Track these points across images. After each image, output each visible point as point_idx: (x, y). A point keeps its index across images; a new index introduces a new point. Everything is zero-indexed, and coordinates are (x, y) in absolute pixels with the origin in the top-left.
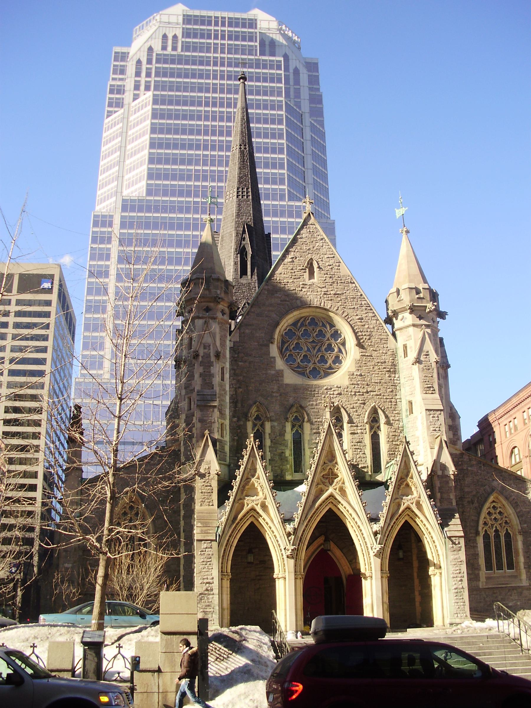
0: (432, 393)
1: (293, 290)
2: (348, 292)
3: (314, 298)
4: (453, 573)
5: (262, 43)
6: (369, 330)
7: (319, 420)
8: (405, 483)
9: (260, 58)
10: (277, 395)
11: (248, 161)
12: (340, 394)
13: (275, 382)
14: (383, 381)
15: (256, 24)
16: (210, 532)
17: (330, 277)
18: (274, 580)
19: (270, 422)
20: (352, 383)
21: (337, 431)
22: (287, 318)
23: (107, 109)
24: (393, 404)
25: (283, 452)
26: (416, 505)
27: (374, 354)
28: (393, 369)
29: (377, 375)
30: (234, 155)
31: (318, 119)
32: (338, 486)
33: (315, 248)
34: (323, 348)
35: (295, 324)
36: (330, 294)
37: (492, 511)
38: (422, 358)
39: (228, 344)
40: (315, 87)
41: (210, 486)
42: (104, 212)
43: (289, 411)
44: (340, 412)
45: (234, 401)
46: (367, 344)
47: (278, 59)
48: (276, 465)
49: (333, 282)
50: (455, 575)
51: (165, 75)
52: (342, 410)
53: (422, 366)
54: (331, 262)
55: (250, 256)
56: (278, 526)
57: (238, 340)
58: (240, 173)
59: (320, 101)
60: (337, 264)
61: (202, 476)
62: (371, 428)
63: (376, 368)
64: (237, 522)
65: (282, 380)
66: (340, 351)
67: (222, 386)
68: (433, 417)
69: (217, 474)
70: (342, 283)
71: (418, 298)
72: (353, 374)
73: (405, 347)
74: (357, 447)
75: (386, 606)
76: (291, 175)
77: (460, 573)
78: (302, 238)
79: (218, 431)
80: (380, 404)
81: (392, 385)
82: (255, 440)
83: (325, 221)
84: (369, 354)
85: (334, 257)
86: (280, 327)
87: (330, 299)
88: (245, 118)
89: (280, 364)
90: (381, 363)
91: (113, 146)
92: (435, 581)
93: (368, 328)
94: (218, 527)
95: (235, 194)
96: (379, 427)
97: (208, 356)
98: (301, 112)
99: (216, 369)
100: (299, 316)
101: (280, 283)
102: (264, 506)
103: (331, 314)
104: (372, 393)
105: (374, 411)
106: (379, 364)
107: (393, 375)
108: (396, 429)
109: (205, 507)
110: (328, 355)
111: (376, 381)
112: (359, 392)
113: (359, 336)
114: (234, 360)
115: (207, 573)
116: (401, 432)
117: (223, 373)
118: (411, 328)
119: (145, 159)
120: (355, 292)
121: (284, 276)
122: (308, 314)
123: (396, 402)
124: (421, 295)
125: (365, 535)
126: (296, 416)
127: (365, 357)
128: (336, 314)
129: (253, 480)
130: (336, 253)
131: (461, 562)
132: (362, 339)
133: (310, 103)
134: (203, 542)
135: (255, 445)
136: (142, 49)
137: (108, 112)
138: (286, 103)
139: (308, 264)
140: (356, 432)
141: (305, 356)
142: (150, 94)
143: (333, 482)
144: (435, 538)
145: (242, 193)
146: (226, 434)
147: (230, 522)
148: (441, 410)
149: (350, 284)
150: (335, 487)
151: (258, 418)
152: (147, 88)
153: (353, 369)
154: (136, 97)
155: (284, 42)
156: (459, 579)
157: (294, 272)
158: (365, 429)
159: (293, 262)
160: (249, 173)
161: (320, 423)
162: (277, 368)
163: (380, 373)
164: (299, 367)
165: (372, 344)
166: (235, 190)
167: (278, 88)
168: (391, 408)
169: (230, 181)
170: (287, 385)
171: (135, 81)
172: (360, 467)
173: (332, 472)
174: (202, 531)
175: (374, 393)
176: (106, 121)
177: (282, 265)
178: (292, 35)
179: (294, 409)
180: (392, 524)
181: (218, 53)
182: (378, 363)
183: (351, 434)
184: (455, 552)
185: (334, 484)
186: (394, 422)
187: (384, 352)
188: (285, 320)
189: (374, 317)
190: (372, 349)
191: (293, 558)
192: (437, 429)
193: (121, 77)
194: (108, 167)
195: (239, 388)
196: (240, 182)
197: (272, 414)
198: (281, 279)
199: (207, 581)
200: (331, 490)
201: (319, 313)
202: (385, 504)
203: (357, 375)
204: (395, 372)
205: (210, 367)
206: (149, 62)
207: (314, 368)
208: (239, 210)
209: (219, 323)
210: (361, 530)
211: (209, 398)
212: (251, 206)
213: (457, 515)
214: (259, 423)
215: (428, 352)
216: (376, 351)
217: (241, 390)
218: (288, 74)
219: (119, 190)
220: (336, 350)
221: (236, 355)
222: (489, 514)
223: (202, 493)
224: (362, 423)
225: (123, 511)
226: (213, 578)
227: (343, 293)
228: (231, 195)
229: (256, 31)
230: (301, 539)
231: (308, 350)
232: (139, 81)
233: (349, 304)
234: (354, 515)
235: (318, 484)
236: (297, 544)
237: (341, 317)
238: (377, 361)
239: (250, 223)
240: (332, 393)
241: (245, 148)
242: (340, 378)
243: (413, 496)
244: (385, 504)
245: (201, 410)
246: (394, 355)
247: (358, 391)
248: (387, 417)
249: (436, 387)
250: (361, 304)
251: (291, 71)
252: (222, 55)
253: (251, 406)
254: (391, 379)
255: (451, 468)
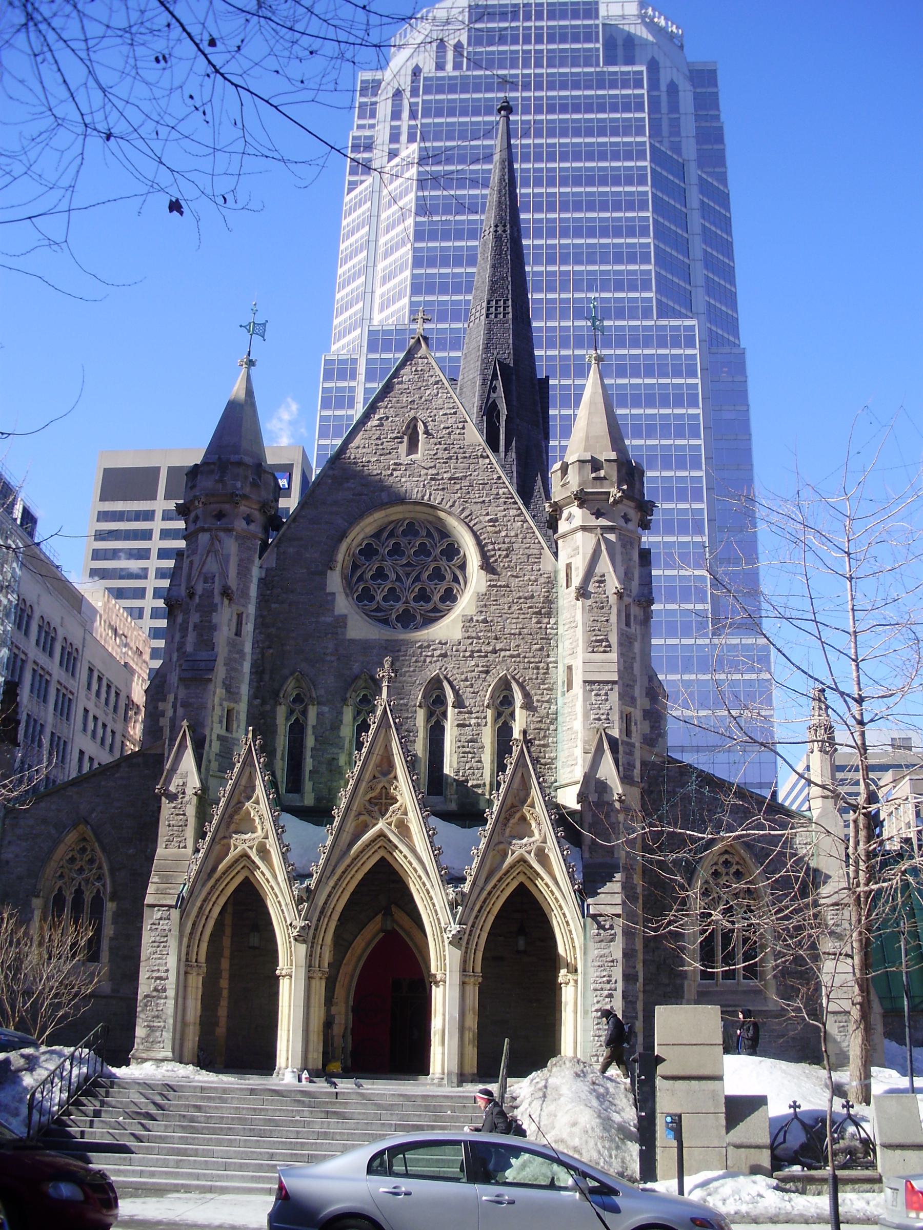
0: (605, 652)
1: (378, 474)
2: (476, 473)
3: (411, 486)
4: (595, 982)
5: (610, 44)
6: (507, 540)
7: (402, 702)
8: (518, 815)
9: (605, 69)
10: (333, 658)
11: (509, 252)
12: (444, 655)
13: (330, 636)
14: (525, 631)
15: (597, 10)
16: (171, 892)
17: (445, 449)
18: (276, 979)
19: (315, 707)
20: (467, 635)
21: (397, 720)
22: (362, 524)
23: (348, 178)
24: (542, 671)
25: (334, 759)
26: (536, 855)
27: (514, 582)
28: (547, 609)
29: (514, 621)
30: (485, 243)
31: (717, 170)
32: (394, 819)
33: (423, 399)
34: (425, 576)
35: (377, 535)
36: (442, 479)
37: (722, 870)
38: (591, 588)
39: (256, 573)
40: (711, 113)
41: (184, 815)
42: (344, 354)
43: (350, 685)
44: (510, 689)
45: (258, 671)
46: (502, 564)
47: (636, 68)
48: (322, 780)
49: (450, 458)
50: (598, 986)
51: (439, 114)
52: (445, 684)
53: (589, 602)
54: (451, 421)
55: (505, 417)
56: (283, 885)
57: (274, 565)
58: (494, 275)
59: (720, 139)
60: (460, 425)
61: (172, 797)
62: (499, 715)
63: (515, 607)
64: (217, 875)
65: (344, 634)
66: (456, 579)
67: (235, 646)
68: (596, 695)
69: (196, 794)
70: (465, 457)
71: (594, 478)
72: (471, 620)
73: (569, 566)
74: (468, 750)
75: (469, 1036)
76: (663, 273)
77: (609, 982)
78: (401, 383)
79: (221, 722)
80: (516, 672)
81: (541, 639)
82: (254, 736)
83: (729, 351)
84: (503, 584)
85: (455, 413)
86: (349, 540)
87: (441, 487)
88: (506, 177)
89: (343, 604)
90: (525, 598)
91: (357, 241)
92: (568, 994)
93: (506, 536)
94: (185, 884)
95: (484, 311)
96: (512, 715)
97: (209, 594)
98: (680, 160)
99: (224, 616)
100: (387, 520)
101: (355, 463)
102: (263, 852)
103: (442, 515)
104: (503, 654)
105: (504, 685)
106: (522, 600)
107: (546, 620)
108: (542, 718)
109: (173, 850)
110: (433, 587)
111: (513, 631)
112: (480, 651)
113: (489, 551)
114: (263, 601)
115: (158, 961)
116: (551, 723)
117: (239, 624)
118: (580, 534)
119: (407, 260)
120: (488, 474)
121: (364, 450)
122: (401, 516)
123: (548, 668)
124: (602, 473)
125: (437, 907)
126: (365, 695)
127: (495, 589)
128: (449, 513)
129: (248, 804)
130: (460, 405)
131: (613, 961)
132: (493, 556)
133: (698, 143)
134: (156, 908)
135: (255, 745)
136: (403, 72)
137: (350, 183)
138: (652, 146)
139: (408, 427)
140: (467, 723)
141: (392, 590)
142: (414, 147)
143: (387, 810)
144: (569, 918)
145: (496, 310)
146: (238, 726)
147: (203, 876)
148: (614, 682)
149: (480, 460)
150: (389, 820)
151: (298, 699)
152: (411, 139)
153: (472, 611)
154: (393, 154)
155: (651, 38)
156: (606, 993)
157: (382, 444)
158: (485, 718)
159: (382, 425)
160: (509, 274)
161: (404, 708)
162: (336, 613)
163: (522, 616)
164: (378, 610)
165: (512, 564)
166: (484, 305)
167: (637, 119)
168: (537, 678)
169: (477, 289)
170: (352, 641)
171: (392, 127)
172: (469, 785)
173: (387, 793)
174: (158, 890)
175: (508, 653)
176: (347, 199)
177: (362, 433)
178: (667, 24)
179: (361, 683)
180: (488, 888)
181: (530, 67)
182: (520, 598)
183: (458, 726)
184: (603, 944)
185: (387, 816)
186: (539, 704)
187: (532, 578)
188: (357, 529)
189: (519, 515)
190: (509, 573)
191: (304, 942)
192: (603, 717)
193: (372, 122)
194: (349, 277)
195: (269, 647)
196: (492, 291)
197: (322, 692)
198: (358, 456)
199: (159, 974)
200: (381, 825)
201: (419, 514)
202: (476, 851)
203: (477, 621)
204: (549, 615)
205: (210, 612)
206: (414, 92)
207: (406, 611)
208: (489, 339)
209: (237, 539)
210: (431, 899)
211: (202, 665)
212: (511, 331)
213: (618, 876)
214: (299, 707)
215: (603, 576)
216: (517, 577)
217: (271, 651)
218: (655, 93)
219: (367, 316)
220: (449, 577)
221: (268, 592)
222: (716, 874)
223: (169, 826)
224: (479, 706)
225: (70, 856)
226: (167, 971)
227: (466, 476)
228: (478, 314)
229: (597, 22)
230: (323, 908)
231: (398, 579)
232: (399, 127)
233: (475, 496)
234: (421, 872)
235: (360, 814)
236: (470, 924)
237: (458, 518)
238: (518, 595)
239: (508, 361)
240: (430, 654)
241: (504, 231)
242: (448, 628)
243: (532, 840)
244: (476, 851)
245: (187, 687)
246: (551, 583)
247: (477, 649)
248: (527, 695)
249: (614, 639)
250: (498, 494)
251: (663, 87)
252: (538, 71)
253: (287, 678)
254: (541, 628)
255: (617, 788)
